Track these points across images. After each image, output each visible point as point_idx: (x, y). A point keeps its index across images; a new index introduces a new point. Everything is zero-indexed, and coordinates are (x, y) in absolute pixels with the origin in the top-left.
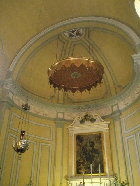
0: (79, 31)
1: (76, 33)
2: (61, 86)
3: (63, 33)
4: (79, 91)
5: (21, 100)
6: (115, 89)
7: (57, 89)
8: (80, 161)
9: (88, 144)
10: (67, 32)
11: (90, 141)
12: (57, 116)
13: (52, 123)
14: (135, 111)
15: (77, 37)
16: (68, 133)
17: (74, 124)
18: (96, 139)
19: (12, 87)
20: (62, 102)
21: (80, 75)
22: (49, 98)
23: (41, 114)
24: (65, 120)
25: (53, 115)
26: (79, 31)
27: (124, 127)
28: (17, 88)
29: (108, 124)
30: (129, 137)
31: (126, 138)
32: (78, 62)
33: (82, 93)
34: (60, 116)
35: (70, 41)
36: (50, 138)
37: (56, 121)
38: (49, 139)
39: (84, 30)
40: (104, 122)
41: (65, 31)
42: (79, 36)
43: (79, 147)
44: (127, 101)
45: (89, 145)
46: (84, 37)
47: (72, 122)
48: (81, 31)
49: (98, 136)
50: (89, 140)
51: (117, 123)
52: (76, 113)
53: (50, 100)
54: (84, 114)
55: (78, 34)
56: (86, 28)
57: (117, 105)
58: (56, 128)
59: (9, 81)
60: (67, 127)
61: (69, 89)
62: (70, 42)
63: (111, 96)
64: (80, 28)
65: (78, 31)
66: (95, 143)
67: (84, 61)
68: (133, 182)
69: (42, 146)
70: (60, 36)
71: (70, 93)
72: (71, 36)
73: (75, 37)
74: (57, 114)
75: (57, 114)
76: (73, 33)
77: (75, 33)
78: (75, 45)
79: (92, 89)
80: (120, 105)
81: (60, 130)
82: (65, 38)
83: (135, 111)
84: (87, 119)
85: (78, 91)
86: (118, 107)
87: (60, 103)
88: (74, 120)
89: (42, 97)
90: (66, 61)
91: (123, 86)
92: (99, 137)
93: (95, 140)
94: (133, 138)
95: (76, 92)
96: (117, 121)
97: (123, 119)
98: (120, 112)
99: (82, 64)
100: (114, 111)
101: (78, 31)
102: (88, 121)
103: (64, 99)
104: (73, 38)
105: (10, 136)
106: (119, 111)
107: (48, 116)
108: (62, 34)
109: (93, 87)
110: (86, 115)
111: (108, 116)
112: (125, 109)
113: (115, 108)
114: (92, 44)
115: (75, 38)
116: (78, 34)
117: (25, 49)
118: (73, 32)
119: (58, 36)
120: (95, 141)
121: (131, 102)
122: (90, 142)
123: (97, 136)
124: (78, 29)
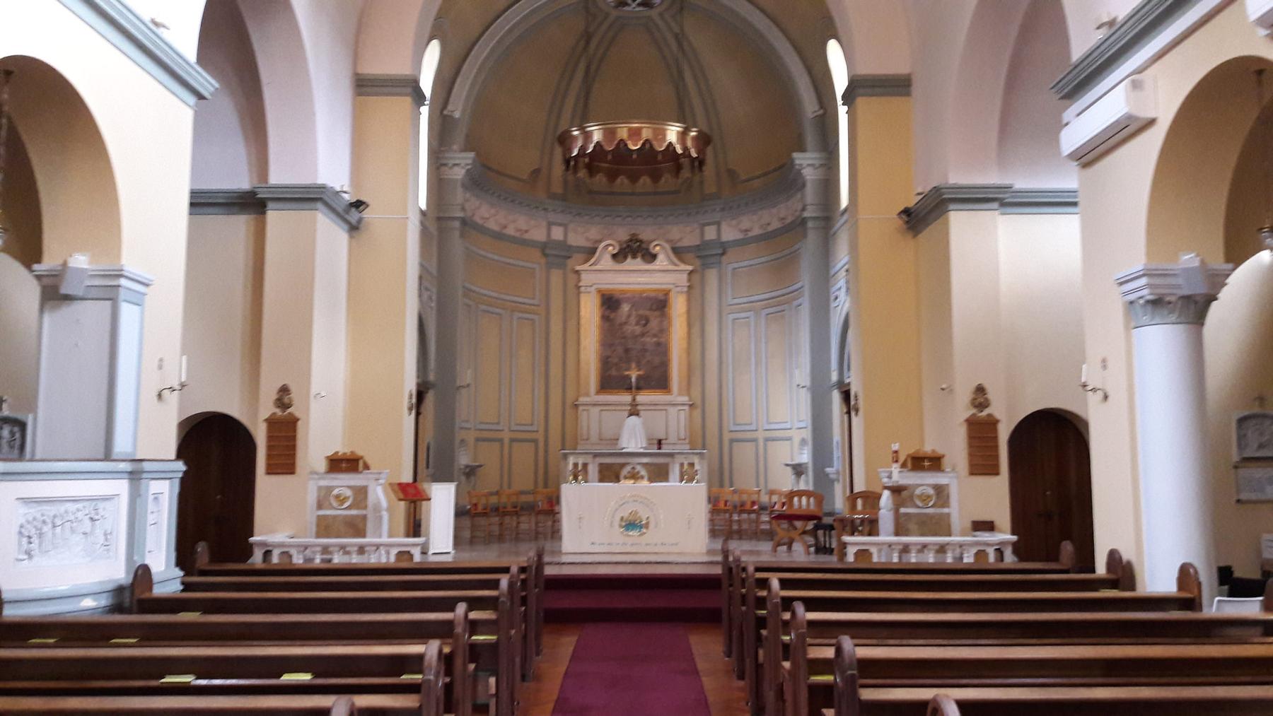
8: (610, 359)
12: (549, 234)
13: (537, 254)
14: (763, 259)
18: (654, 307)
23: (510, 231)
25: (539, 235)
27: (731, 367)
30: (742, 263)
31: (731, 317)
34: (557, 233)
36: (533, 299)
37: (548, 251)
40: (676, 265)
44: (746, 222)
46: (661, 15)
51: (712, 276)
54: (623, 234)
57: (718, 224)
59: (465, 158)
60: (578, 268)
74: (549, 230)
75: (549, 230)
80: (724, 227)
81: (556, 276)
83: (763, 259)
84: (634, 249)
86: (719, 231)
88: (597, 248)
91: (743, 177)
92: (660, 304)
96: (712, 268)
98: (724, 248)
102: (637, 258)
107: (526, 236)
111: (688, 249)
112: (737, 243)
113: (710, 233)
117: (488, 50)
121: (757, 231)
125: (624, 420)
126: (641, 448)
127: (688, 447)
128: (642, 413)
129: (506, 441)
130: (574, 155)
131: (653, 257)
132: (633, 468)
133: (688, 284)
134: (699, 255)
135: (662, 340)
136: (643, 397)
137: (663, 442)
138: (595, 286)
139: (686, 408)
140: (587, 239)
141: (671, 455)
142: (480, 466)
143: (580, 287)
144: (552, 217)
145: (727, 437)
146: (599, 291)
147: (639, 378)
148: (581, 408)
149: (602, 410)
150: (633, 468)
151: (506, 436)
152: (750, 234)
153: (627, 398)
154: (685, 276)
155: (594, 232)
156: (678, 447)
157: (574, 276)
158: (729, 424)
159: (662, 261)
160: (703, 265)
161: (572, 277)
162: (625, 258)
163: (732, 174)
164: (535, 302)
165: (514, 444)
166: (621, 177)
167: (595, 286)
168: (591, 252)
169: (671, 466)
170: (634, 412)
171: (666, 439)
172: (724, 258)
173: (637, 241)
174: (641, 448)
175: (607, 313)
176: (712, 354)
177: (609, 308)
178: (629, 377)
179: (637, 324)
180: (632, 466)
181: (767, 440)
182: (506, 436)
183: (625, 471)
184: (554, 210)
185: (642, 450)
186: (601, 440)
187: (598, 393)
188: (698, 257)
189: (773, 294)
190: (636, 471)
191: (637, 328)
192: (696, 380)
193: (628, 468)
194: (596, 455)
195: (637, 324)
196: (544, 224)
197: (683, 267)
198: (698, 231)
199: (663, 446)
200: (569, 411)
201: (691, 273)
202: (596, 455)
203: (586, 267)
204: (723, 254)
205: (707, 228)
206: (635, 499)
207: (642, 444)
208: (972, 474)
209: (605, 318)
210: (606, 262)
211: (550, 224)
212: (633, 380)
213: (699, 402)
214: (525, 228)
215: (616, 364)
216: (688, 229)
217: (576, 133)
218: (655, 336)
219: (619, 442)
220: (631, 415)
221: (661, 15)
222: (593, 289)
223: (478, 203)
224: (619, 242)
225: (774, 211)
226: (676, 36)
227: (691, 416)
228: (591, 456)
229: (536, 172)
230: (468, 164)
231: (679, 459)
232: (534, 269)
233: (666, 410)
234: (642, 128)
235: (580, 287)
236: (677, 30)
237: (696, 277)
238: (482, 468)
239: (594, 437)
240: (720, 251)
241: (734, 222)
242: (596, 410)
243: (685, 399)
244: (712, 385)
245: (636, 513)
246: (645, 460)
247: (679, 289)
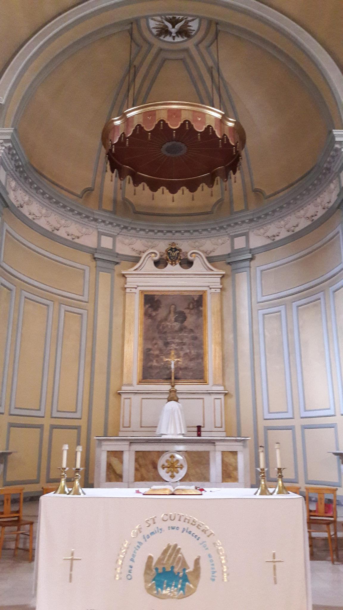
0: (190, 24)
1: (181, 28)
2: (124, 167)
3: (147, 18)
4: (148, 185)
5: (20, 192)
6: (245, 196)
7: (131, 181)
8: (152, 352)
9: (172, 317)
10: (159, 18)
11: (175, 309)
13: (88, 258)
15: (179, 39)
16: (126, 286)
17: (140, 266)
18: (191, 306)
19: (7, 151)
20: (110, 208)
21: (185, 149)
22: (79, 193)
23: (62, 233)
24: (118, 254)
25: (90, 241)
26: (190, 24)
28: (17, 158)
29: (220, 276)
32: (199, 119)
33: (175, 195)
34: (107, 243)
35: (157, 44)
36: (83, 296)
37: (96, 256)
38: (80, 298)
39: (205, 24)
41: (152, 17)
42: (185, 38)
43: (150, 320)
45: (173, 319)
46: (197, 45)
47: (138, 262)
48: (194, 25)
49: (196, 299)
50: (173, 306)
51: (242, 279)
52: (144, 241)
53: (81, 198)
55: (184, 32)
56: (210, 22)
57: (246, 235)
58: (96, 273)
60: (123, 272)
61: (143, 180)
62: (154, 50)
63: (232, 212)
64: (197, 17)
65: (187, 22)
66: (188, 316)
67: (166, 111)
68: (268, 401)
69: (65, 313)
70: (134, 26)
71: (129, 187)
72: (164, 31)
73: (174, 37)
76: (173, 27)
77: (178, 26)
78: (164, 60)
79: (200, 188)
81: (104, 278)
82: (147, 34)
85: (165, 188)
86: (247, 241)
87: (106, 211)
88: (140, 258)
89: (62, 188)
90: (169, 110)
91: (268, 194)
93: (188, 308)
94: (280, 313)
95: (160, 190)
97: (259, 269)
98: (253, 254)
99: (209, 126)
100: (236, 247)
101: (187, 22)
102: (176, 264)
103: (115, 201)
104: (168, 39)
105: (26, 297)
106: (251, 250)
108: (143, 23)
109: (204, 184)
110: (171, 249)
112: (266, 248)
113: (240, 243)
114: (212, 68)
115: (172, 41)
116: (184, 32)
118: (174, 22)
119: (132, 23)
120: (187, 311)
121: (284, 234)
122: (175, 313)
123: (193, 299)
124: (190, 18)
125: (164, 406)
126: (180, 434)
127: (224, 434)
128: (179, 400)
129: (47, 429)
130: (115, 143)
131: (189, 264)
132: (172, 476)
133: (221, 287)
134: (229, 261)
135: (198, 335)
136: (179, 387)
137: (202, 429)
138: (139, 288)
139: (222, 396)
140: (134, 250)
141: (212, 442)
142: (10, 453)
143: (126, 288)
144: (102, 227)
145: (261, 424)
146: (142, 292)
147: (178, 369)
148: (123, 396)
149: (143, 399)
150: (172, 457)
151: (47, 422)
152: (277, 239)
153: (166, 387)
154: (219, 279)
155: (139, 244)
156: (213, 434)
157: (122, 279)
158: (263, 412)
159: (198, 266)
160: (232, 270)
161: (119, 281)
162: (166, 265)
163: (257, 192)
164: (85, 298)
165: (55, 430)
166: (162, 188)
167: (139, 288)
168: (136, 260)
169: (211, 455)
170: (173, 397)
171: (204, 427)
172: (252, 263)
173: (176, 249)
174: (180, 434)
175: (150, 310)
176: (245, 347)
177: (151, 307)
178: (169, 363)
179: (176, 321)
180: (170, 454)
181: (304, 427)
182: (47, 422)
183: (162, 461)
184: (104, 221)
185: (181, 437)
186: (141, 427)
187: (140, 382)
188: (229, 263)
189: (302, 288)
190: (175, 460)
191: (175, 324)
192: (230, 370)
193: (166, 457)
194: (132, 442)
195: (176, 321)
196: (95, 233)
197: (216, 271)
198: (229, 242)
199: (203, 434)
200: (112, 398)
201: (223, 276)
202: (132, 442)
203: (131, 271)
204: (251, 259)
205: (236, 240)
206: (175, 524)
207: (181, 431)
208: (43, 425)
209: (147, 315)
210: (149, 266)
211: (100, 234)
212: (173, 366)
213: (233, 392)
214: (77, 234)
215: (157, 356)
216: (220, 241)
217: (118, 123)
218: (192, 331)
219: (158, 429)
220: (169, 400)
221: (197, 45)
222: (137, 291)
223: (27, 198)
224: (160, 253)
225: (302, 212)
226: (210, 70)
227: (225, 403)
228: (128, 443)
229: (88, 191)
230: (6, 141)
231: (221, 447)
232: (84, 270)
233: (203, 399)
234: (180, 110)
235: (126, 288)
236: (210, 63)
237: (228, 281)
238: (11, 455)
239: (135, 425)
240: (250, 256)
241: (262, 231)
242: (136, 399)
243: (221, 388)
244: (245, 374)
245: (176, 550)
246: (181, 448)
247: (213, 290)
